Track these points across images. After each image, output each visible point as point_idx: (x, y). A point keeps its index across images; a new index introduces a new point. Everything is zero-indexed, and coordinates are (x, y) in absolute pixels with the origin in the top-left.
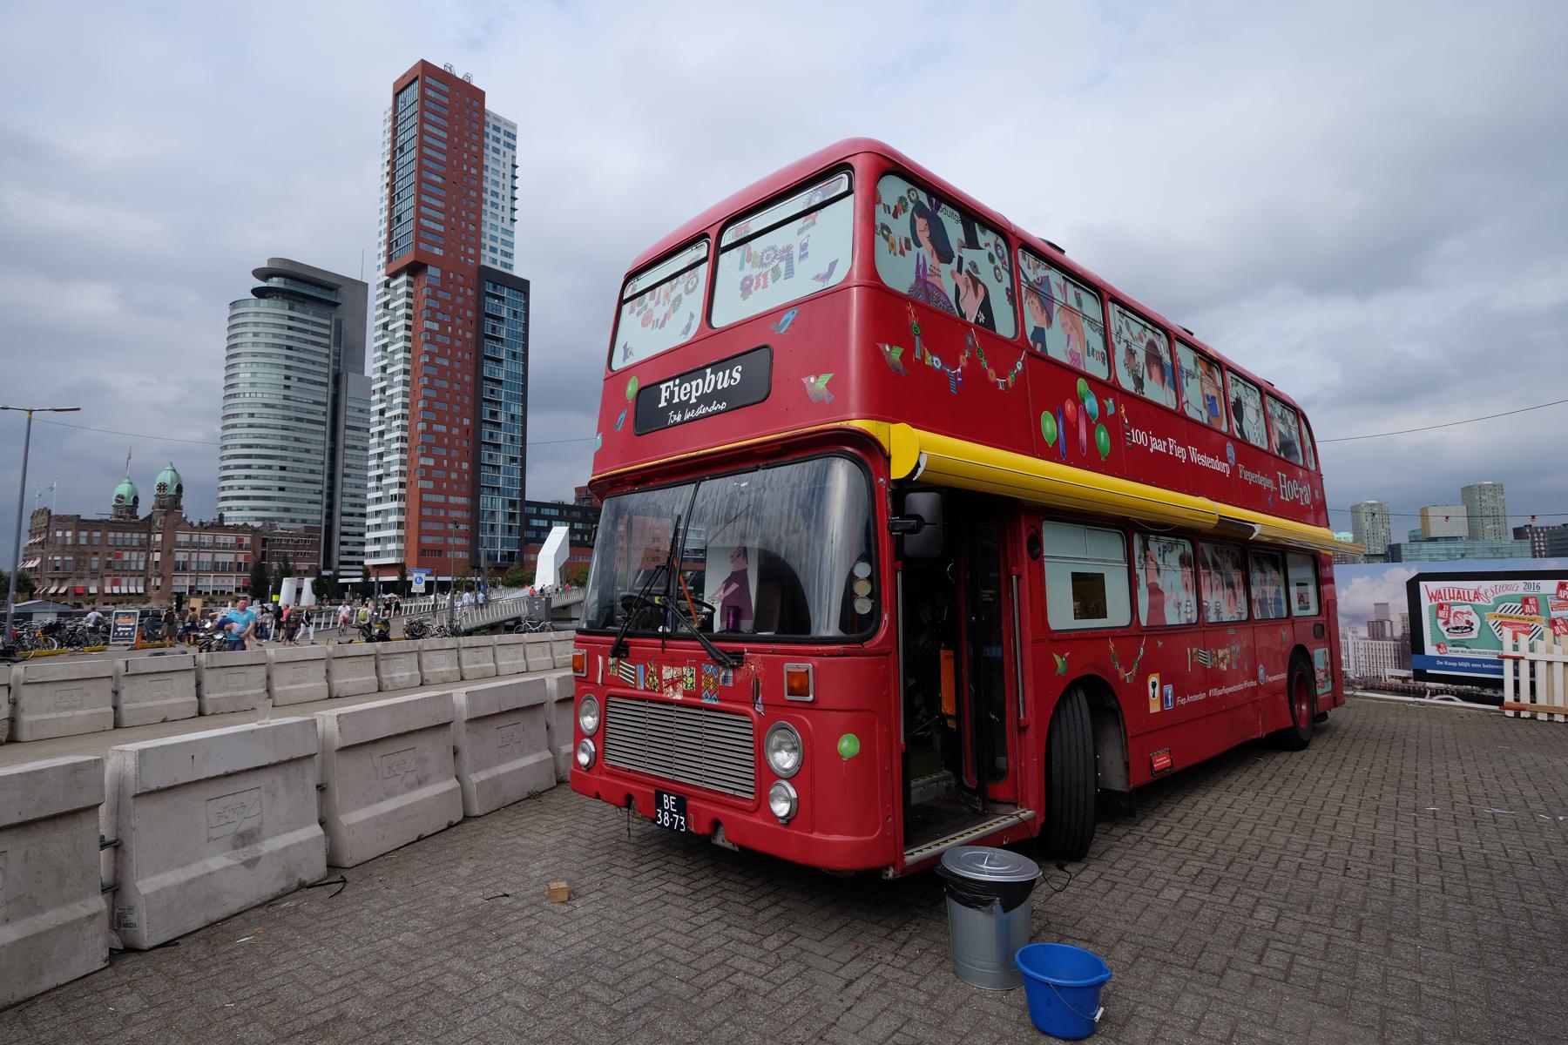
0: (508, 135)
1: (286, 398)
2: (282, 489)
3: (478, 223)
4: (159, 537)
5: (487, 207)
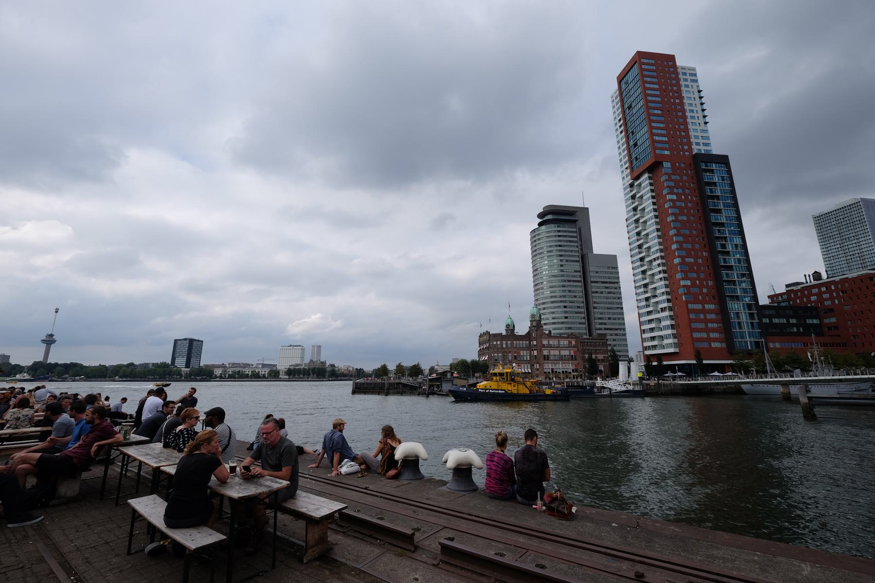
0: (691, 75)
1: (562, 271)
2: (566, 318)
3: (687, 130)
4: (535, 343)
5: (689, 120)
